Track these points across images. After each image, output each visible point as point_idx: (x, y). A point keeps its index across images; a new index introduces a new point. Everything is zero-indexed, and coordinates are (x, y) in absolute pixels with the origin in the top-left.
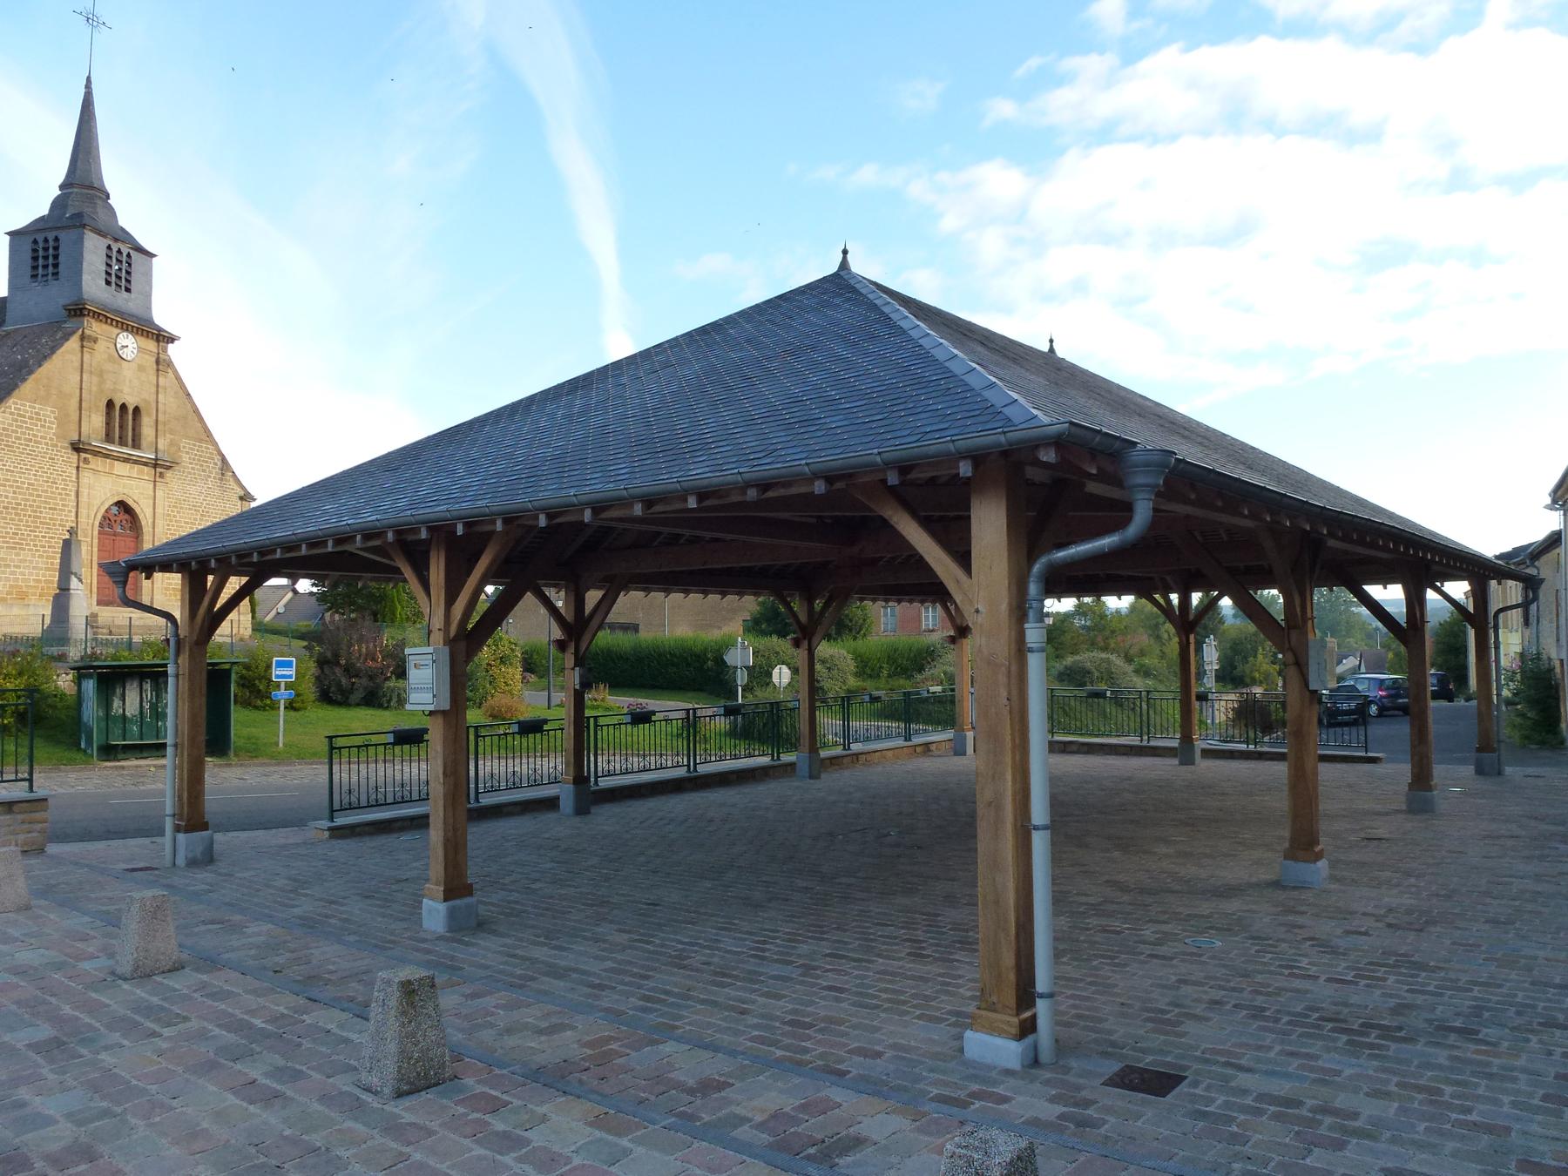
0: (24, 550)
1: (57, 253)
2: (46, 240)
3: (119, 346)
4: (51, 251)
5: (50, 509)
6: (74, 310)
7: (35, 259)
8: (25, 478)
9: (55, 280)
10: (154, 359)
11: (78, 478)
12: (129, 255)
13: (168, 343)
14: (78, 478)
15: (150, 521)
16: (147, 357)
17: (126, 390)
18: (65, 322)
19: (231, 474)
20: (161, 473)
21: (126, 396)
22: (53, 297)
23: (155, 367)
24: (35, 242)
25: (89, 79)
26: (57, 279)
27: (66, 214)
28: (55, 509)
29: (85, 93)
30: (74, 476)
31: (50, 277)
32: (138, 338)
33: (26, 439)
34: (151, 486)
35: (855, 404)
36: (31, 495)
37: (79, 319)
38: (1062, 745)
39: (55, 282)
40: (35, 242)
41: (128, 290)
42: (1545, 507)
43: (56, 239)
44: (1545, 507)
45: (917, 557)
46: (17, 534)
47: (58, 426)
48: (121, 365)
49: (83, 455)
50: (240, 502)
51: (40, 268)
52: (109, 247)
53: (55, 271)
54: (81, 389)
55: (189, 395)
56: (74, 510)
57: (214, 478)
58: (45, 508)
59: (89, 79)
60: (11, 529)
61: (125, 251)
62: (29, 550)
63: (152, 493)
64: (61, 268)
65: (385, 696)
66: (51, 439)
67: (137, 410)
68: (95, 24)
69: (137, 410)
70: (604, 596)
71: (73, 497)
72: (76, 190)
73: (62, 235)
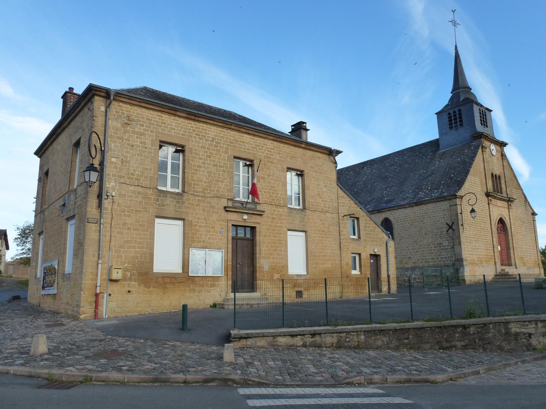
1: (461, 116)
2: (455, 112)
3: (491, 150)
4: (458, 116)
6: (477, 136)
7: (450, 121)
9: (462, 127)
10: (500, 154)
11: (489, 208)
12: (485, 112)
13: (504, 147)
14: (489, 208)
15: (509, 224)
17: (496, 169)
18: (472, 142)
19: (528, 203)
20: (510, 204)
21: (496, 171)
22: (463, 134)
23: (501, 157)
24: (449, 114)
25: (456, 46)
26: (463, 127)
27: (460, 100)
29: (455, 52)
30: (488, 207)
31: (459, 126)
32: (496, 146)
34: (507, 210)
35: (247, 125)
37: (480, 140)
38: (527, 312)
39: (461, 128)
40: (449, 114)
41: (487, 127)
43: (460, 110)
45: (39, 155)
47: (481, 186)
48: (492, 158)
49: (490, 198)
50: (532, 216)
51: (453, 124)
52: (480, 110)
53: (461, 123)
54: (485, 169)
55: (512, 169)
56: (490, 223)
59: (456, 46)
61: (484, 110)
63: (508, 213)
64: (464, 121)
67: (499, 176)
68: (453, 22)
70: (537, 246)
71: (488, 217)
72: (461, 90)
73: (462, 108)
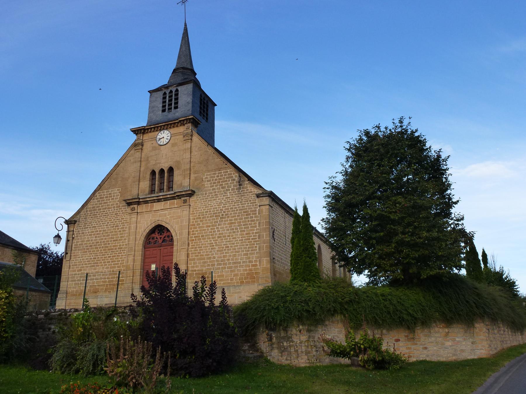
0: (99, 266)
5: (114, 241)
8: (199, 210)
16: (177, 137)
17: (163, 161)
28: (117, 240)
33: (103, 209)
36: (104, 236)
42: (148, 91)
43: (177, 90)
44: (148, 91)
46: (95, 258)
57: (233, 189)
58: (111, 241)
59: (185, 23)
60: (93, 256)
62: (102, 265)
65: (67, 351)
66: (117, 204)
69: (171, 170)
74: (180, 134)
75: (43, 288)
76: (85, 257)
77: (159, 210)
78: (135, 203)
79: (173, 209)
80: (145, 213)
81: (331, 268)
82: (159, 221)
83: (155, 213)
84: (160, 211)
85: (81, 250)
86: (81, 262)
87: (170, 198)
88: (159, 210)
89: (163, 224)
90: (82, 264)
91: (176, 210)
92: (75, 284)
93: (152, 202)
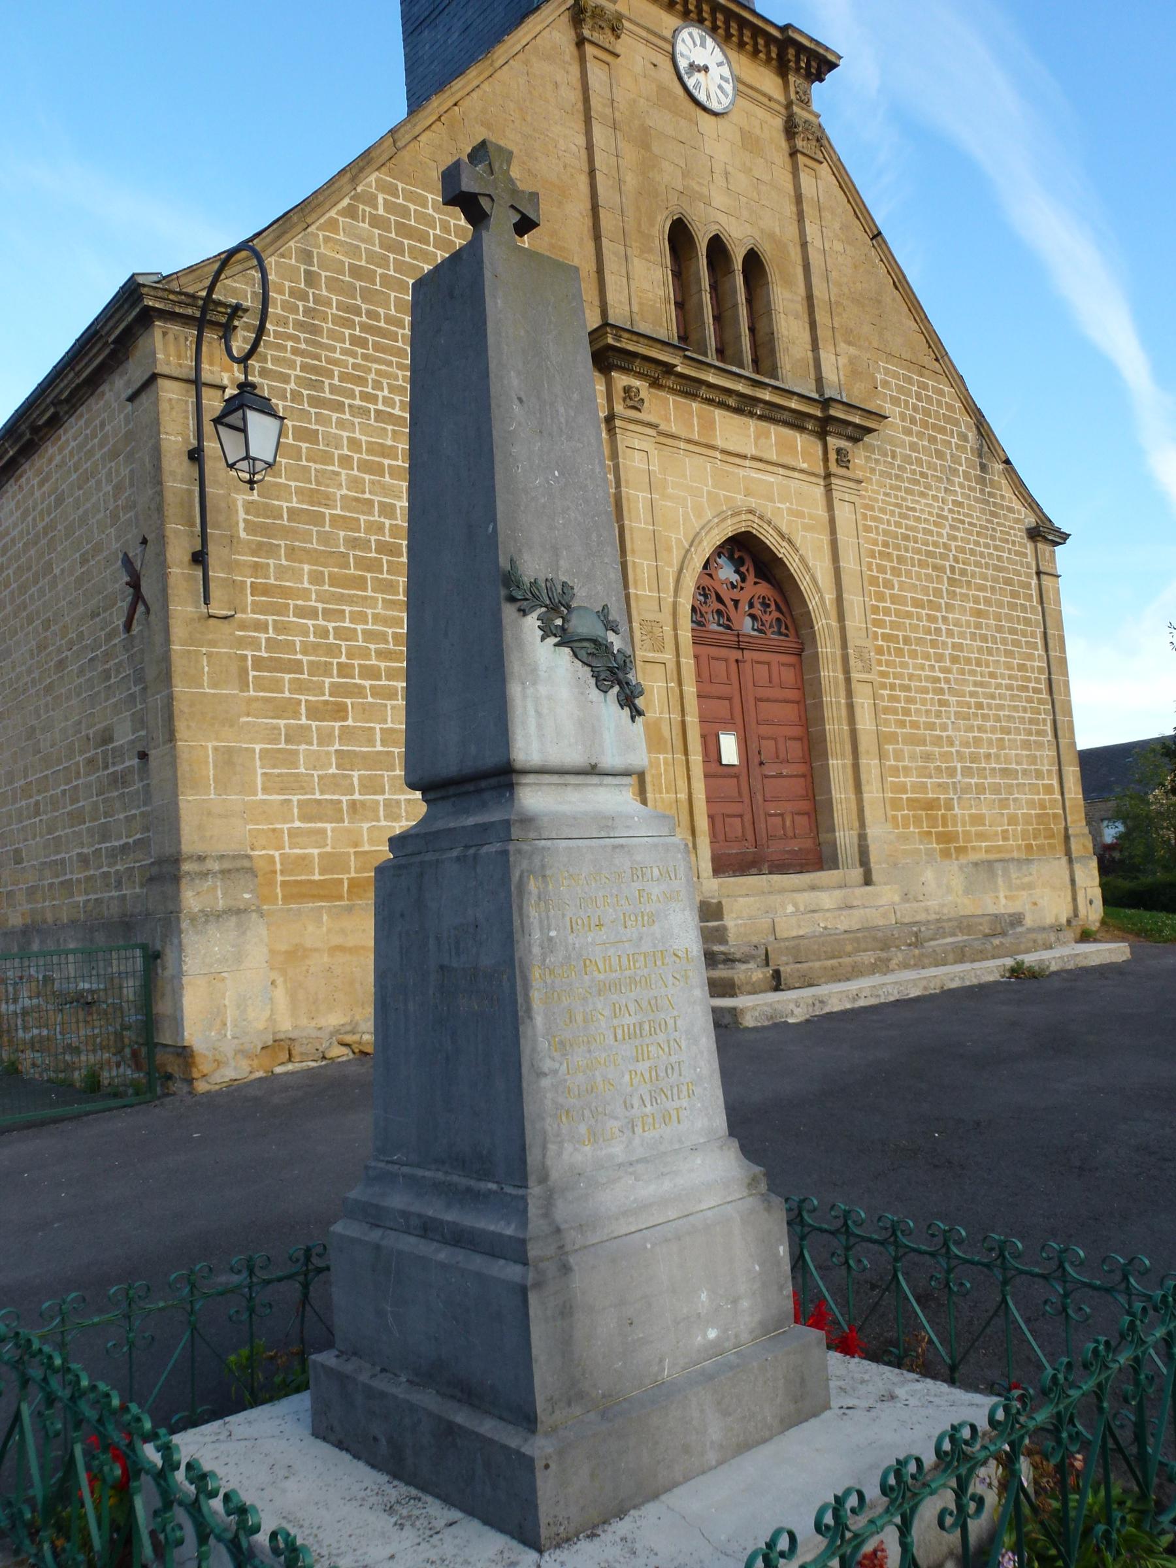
57: (966, 476)
74: (765, 101)
75: (144, 290)
76: (360, 618)
77: (745, 457)
78: (647, 368)
79: (796, 475)
80: (682, 445)
81: (387, 510)
82: (751, 517)
83: (727, 467)
84: (747, 463)
85: (313, 557)
86: (333, 650)
87: (786, 416)
88: (745, 457)
89: (770, 539)
90: (344, 670)
91: (805, 486)
92: (311, 812)
93: (709, 401)
